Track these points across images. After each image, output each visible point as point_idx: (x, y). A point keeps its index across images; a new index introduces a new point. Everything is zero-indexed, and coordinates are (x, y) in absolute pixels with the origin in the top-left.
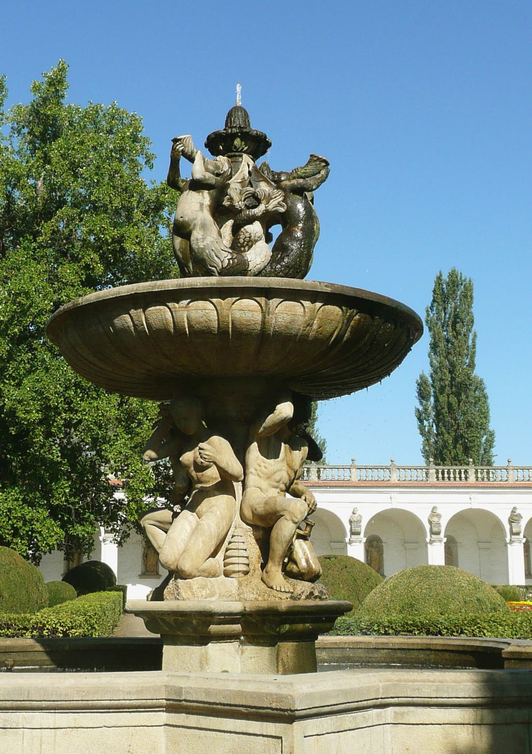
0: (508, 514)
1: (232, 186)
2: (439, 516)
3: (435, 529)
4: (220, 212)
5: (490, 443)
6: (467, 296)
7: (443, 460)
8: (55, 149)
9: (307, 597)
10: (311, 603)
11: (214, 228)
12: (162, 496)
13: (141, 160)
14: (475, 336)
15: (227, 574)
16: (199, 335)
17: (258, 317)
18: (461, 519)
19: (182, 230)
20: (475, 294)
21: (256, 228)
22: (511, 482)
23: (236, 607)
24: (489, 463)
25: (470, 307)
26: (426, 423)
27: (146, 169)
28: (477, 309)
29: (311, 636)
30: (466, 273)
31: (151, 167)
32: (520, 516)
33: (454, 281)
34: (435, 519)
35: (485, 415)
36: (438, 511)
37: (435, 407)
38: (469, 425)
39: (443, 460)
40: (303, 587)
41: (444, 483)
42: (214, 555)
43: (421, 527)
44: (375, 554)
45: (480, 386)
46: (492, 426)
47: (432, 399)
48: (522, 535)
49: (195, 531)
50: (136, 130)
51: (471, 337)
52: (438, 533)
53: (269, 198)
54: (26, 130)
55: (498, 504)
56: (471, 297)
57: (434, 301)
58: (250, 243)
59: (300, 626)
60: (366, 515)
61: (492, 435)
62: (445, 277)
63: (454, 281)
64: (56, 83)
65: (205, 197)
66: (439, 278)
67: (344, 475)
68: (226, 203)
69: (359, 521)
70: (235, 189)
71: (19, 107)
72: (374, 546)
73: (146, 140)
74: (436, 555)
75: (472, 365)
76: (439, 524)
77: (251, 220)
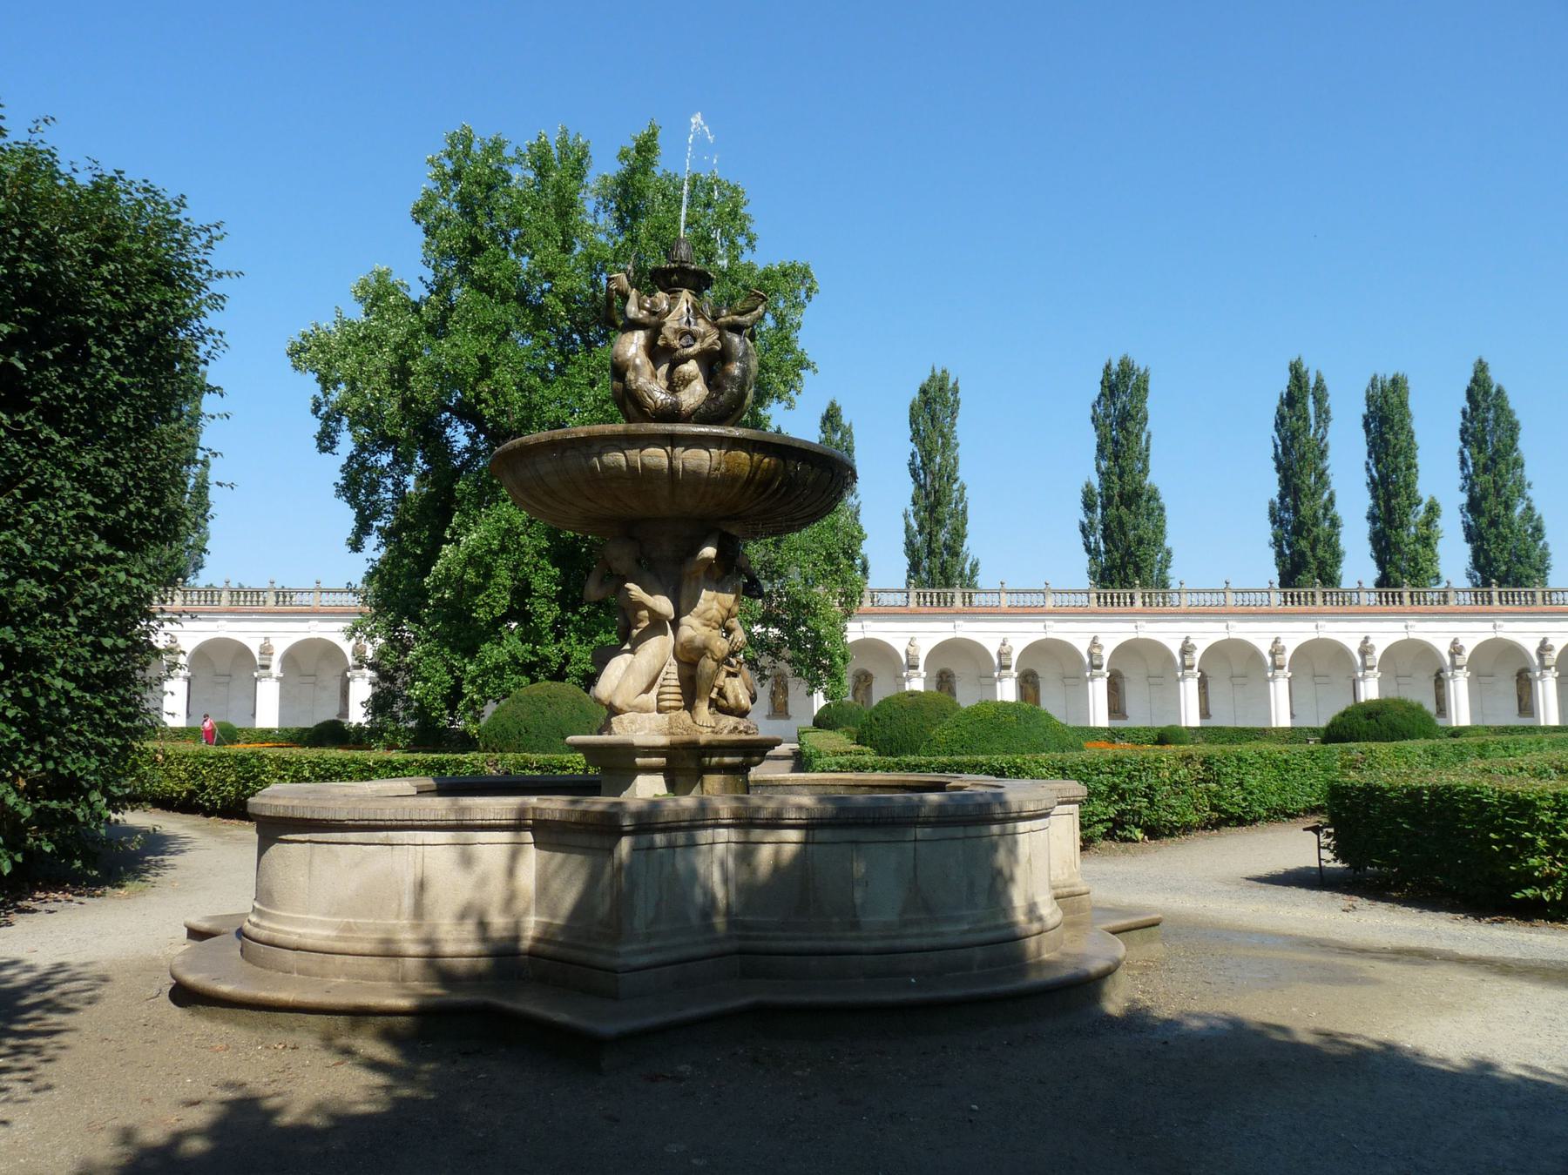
0: (1087, 645)
1: (669, 324)
2: (1100, 647)
3: (1096, 662)
4: (657, 352)
5: (1166, 563)
6: (1141, 388)
7: (1112, 582)
8: (643, 227)
9: (730, 732)
10: (735, 737)
11: (649, 367)
12: (776, 626)
13: (741, 241)
14: (1149, 436)
15: (660, 711)
16: (649, 474)
17: (666, 462)
18: (1128, 650)
19: (619, 370)
20: (1150, 386)
21: (691, 367)
22: (1183, 608)
23: (662, 740)
24: (1165, 585)
25: (1143, 401)
26: (1092, 539)
27: (747, 251)
28: (1153, 404)
29: (742, 770)
30: (1140, 364)
31: (753, 248)
32: (1193, 647)
33: (1126, 369)
34: (1096, 651)
35: (1160, 530)
36: (1100, 642)
37: (1102, 521)
38: (1140, 541)
39: (1112, 582)
40: (731, 721)
41: (1107, 608)
42: (647, 690)
43: (1081, 660)
44: (1030, 691)
45: (1153, 496)
46: (1168, 543)
47: (1099, 510)
48: (1104, 669)
49: (629, 667)
50: (736, 206)
51: (1144, 437)
52: (1008, 667)
53: (704, 336)
54: (613, 205)
55: (1168, 634)
56: (1146, 390)
57: (1102, 394)
58: (686, 382)
59: (727, 760)
60: (1018, 646)
61: (1169, 553)
62: (1115, 367)
63: (1126, 369)
64: (646, 148)
65: (639, 337)
66: (1108, 367)
67: (992, 599)
68: (660, 343)
69: (1008, 654)
70: (671, 323)
71: (605, 178)
72: (1028, 682)
73: (745, 217)
74: (1007, 691)
75: (1145, 471)
76: (1100, 657)
77: (685, 360)
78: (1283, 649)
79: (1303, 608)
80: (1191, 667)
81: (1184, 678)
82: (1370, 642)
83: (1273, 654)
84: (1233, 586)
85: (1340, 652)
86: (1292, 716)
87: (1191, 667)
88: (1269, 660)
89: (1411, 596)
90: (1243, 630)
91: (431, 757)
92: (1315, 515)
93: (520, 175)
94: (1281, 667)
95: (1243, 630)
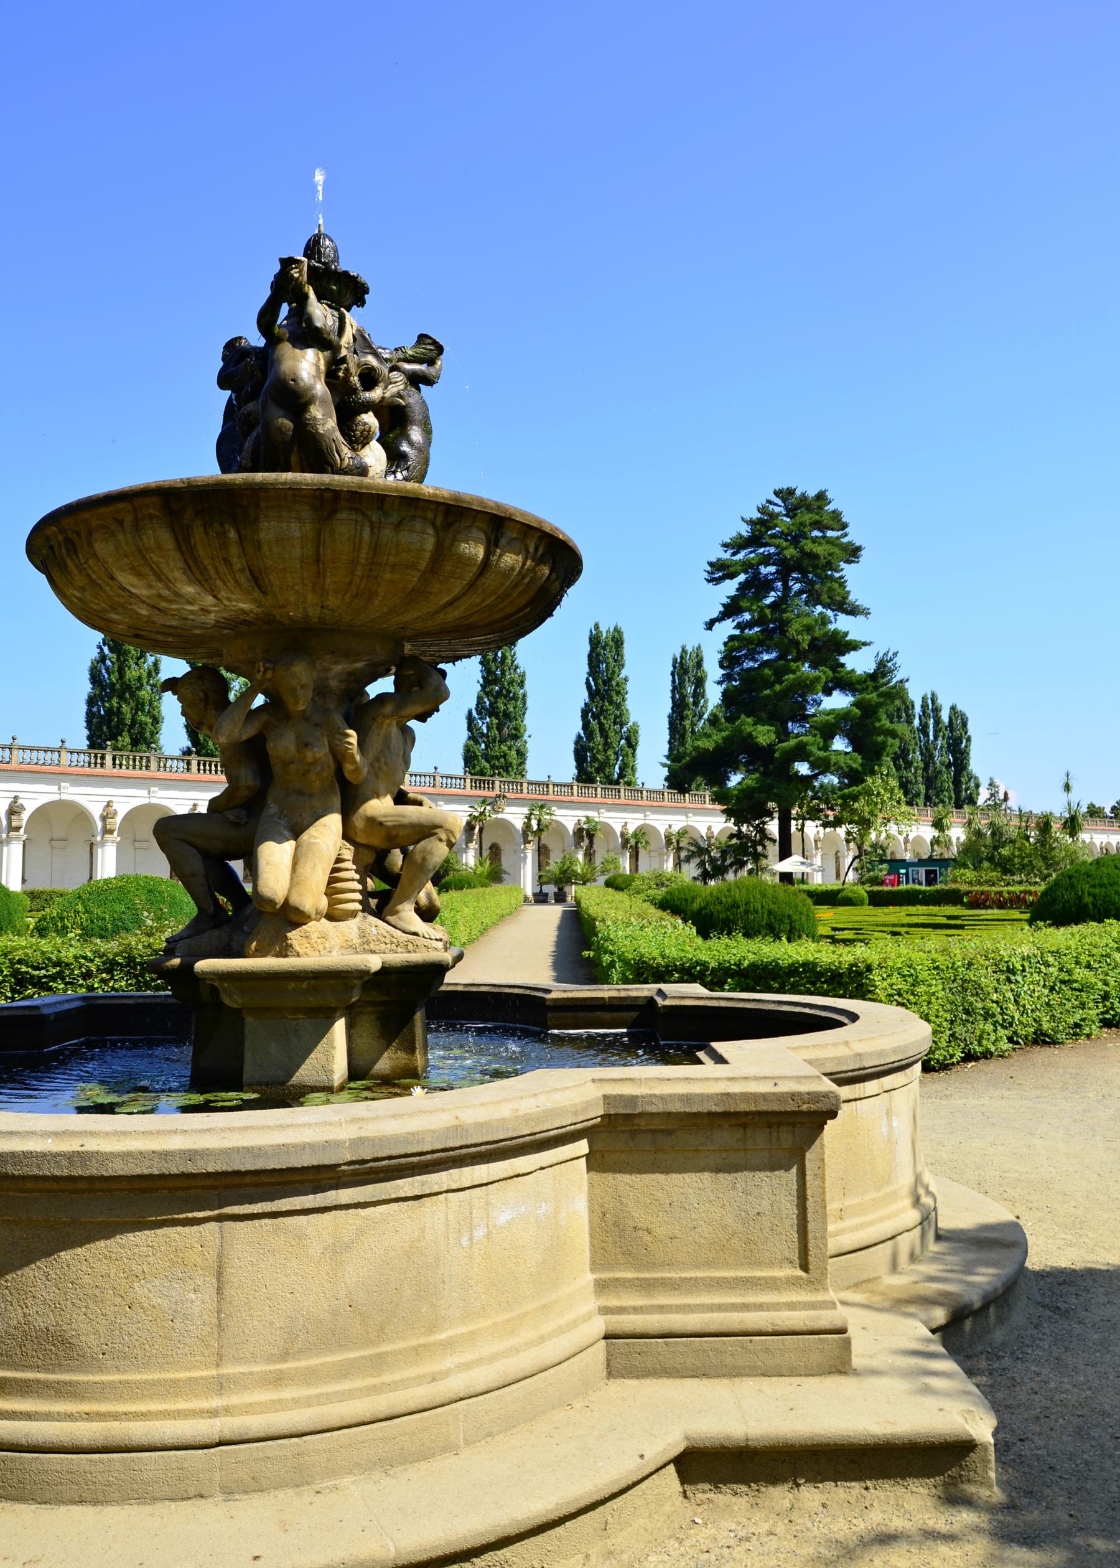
22: (14, 765)
32: (23, 808)
78: (115, 813)
79: (137, 773)
80: (18, 829)
81: (9, 841)
82: (20, 801)
83: (104, 818)
84: (441, 771)
85: (80, 815)
86: (24, 881)
87: (18, 829)
88: (99, 824)
89: (114, 759)
90: (73, 793)
91: (880, 888)
92: (140, 679)
93: (837, 575)
94: (111, 832)
95: (73, 793)
